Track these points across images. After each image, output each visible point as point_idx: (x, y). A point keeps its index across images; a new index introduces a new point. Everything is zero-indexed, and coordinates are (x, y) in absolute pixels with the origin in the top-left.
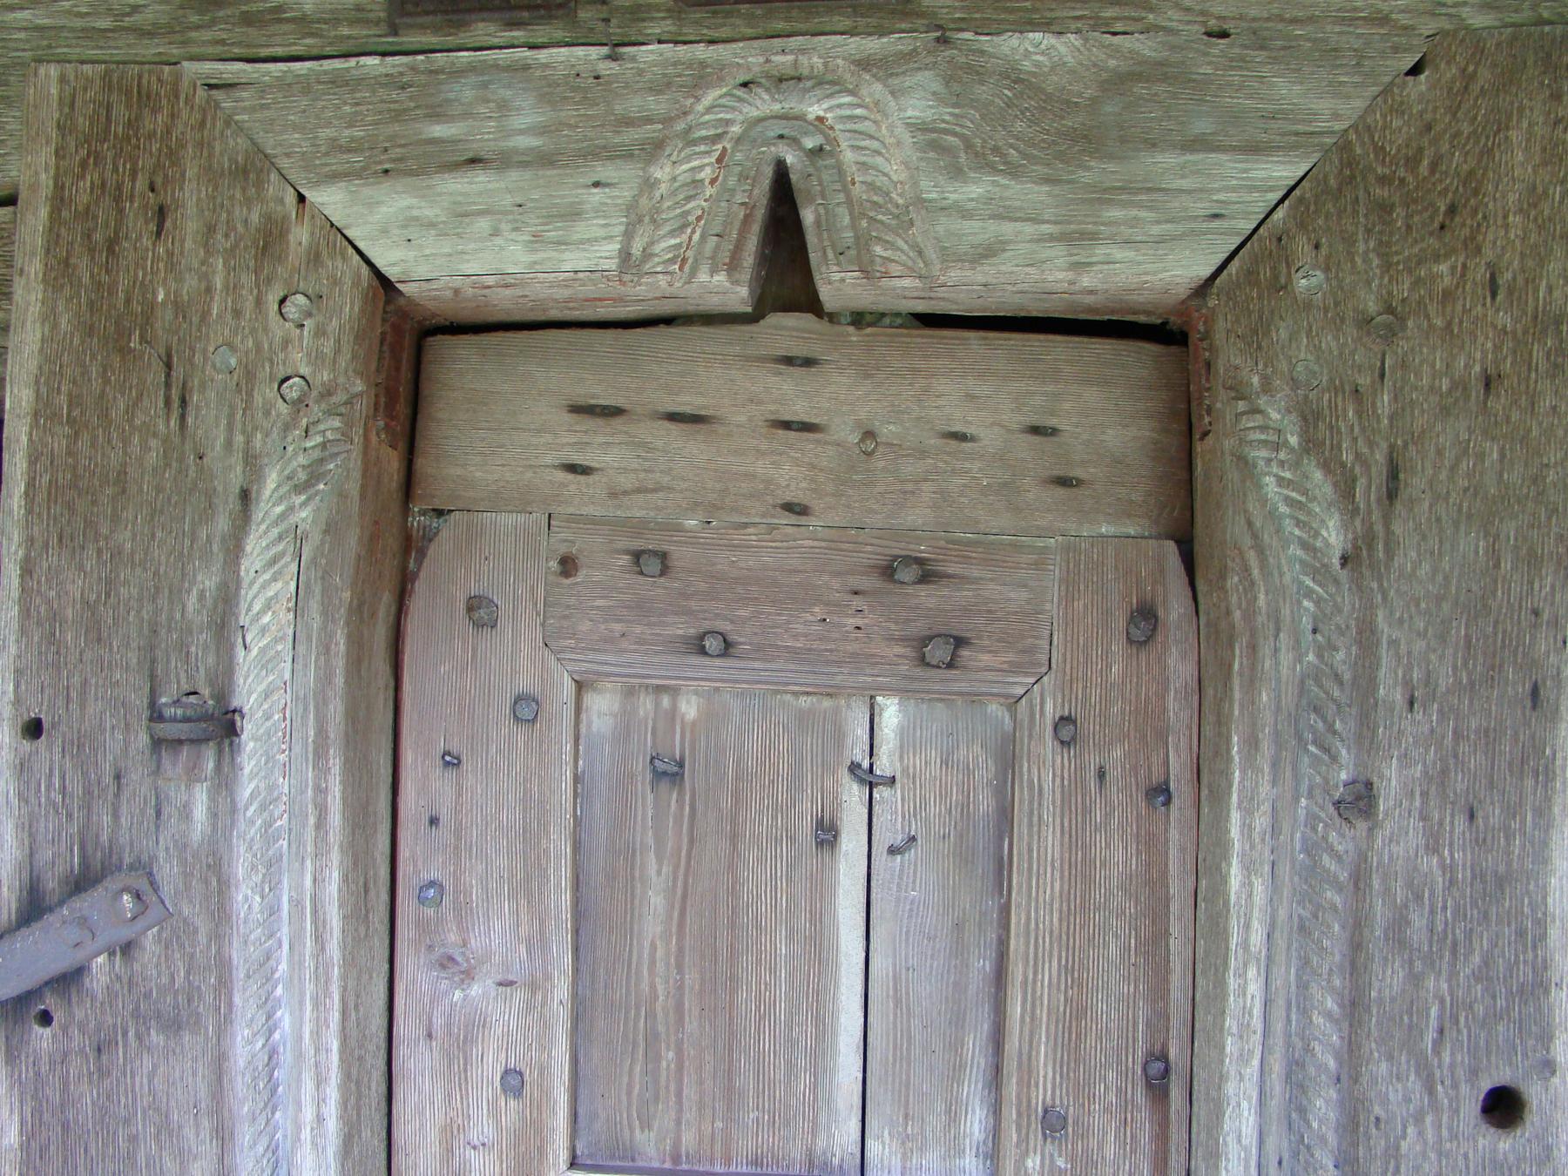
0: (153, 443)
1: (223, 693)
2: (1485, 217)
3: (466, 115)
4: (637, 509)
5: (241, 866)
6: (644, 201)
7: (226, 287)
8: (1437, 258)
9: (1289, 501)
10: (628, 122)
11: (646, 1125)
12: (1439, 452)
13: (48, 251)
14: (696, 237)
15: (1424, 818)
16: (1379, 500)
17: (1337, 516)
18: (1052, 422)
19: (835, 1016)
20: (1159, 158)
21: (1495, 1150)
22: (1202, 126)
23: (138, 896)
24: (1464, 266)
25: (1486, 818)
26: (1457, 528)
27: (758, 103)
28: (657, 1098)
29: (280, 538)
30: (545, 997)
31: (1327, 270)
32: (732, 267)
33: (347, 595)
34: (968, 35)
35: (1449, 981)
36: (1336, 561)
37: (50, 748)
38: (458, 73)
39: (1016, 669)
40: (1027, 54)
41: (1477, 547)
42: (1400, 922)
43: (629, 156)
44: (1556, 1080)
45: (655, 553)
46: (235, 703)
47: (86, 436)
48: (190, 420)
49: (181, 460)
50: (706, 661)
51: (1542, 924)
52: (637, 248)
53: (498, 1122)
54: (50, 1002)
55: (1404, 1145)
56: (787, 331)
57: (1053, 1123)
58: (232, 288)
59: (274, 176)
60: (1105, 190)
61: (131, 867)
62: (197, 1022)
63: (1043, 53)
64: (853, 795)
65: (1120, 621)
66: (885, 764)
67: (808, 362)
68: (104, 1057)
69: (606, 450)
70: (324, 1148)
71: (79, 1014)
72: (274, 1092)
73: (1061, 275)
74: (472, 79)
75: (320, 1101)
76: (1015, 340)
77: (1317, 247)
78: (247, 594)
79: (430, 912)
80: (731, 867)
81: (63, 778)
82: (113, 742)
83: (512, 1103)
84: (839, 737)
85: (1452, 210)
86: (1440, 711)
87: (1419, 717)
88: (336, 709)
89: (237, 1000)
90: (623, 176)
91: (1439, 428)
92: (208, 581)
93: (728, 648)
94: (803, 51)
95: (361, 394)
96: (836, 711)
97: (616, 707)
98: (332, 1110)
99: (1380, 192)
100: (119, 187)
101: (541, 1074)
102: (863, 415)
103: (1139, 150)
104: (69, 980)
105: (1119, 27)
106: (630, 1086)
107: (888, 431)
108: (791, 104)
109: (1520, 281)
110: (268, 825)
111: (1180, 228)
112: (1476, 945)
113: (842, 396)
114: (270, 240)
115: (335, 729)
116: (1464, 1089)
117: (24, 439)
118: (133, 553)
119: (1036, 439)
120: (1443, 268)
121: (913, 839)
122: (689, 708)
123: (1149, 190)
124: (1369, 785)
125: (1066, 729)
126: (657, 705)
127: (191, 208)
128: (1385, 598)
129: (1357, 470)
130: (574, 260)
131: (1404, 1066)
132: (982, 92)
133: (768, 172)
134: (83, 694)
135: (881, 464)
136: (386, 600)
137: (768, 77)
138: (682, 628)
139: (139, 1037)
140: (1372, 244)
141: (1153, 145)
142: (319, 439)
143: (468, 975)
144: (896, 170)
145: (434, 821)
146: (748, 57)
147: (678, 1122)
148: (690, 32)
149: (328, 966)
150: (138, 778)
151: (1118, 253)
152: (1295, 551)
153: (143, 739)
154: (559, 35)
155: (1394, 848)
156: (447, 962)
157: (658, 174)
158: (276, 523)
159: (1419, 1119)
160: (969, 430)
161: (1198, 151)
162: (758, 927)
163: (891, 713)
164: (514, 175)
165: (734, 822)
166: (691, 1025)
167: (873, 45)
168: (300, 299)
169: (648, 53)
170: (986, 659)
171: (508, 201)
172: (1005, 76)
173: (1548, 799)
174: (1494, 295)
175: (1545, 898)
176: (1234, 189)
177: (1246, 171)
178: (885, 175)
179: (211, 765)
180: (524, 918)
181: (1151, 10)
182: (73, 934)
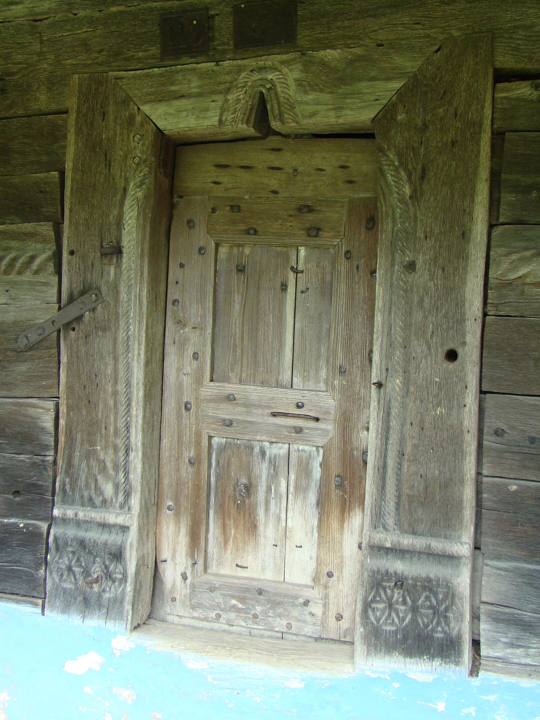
0: (102, 176)
1: (119, 242)
2: (454, 94)
3: (180, 84)
4: (232, 194)
5: (123, 289)
6: (225, 105)
7: (120, 134)
8: (439, 108)
9: (394, 181)
10: (221, 83)
11: (233, 371)
12: (438, 165)
13: (76, 125)
14: (239, 114)
15: (429, 271)
16: (419, 180)
17: (408, 185)
18: (347, 164)
19: (285, 341)
20: (362, 84)
21: (448, 368)
22: (373, 73)
23: (96, 295)
24: (447, 109)
25: (448, 271)
26: (442, 187)
27: (255, 76)
28: (236, 364)
29: (133, 200)
30: (205, 332)
31: (407, 113)
32: (247, 123)
33: (150, 215)
34: (310, 52)
35: (436, 318)
36: (407, 198)
37: (76, 256)
38: (178, 72)
39: (335, 237)
40: (326, 56)
41: (448, 192)
42: (421, 301)
43: (221, 93)
44: (466, 348)
45: (236, 206)
46: (122, 245)
47: (85, 175)
48: (111, 170)
49: (109, 180)
50: (250, 236)
51: (463, 302)
52: (224, 119)
53: (191, 368)
54: (75, 325)
55: (421, 365)
56: (273, 141)
57: (342, 371)
58: (122, 134)
59: (132, 103)
60: (346, 94)
61: (95, 289)
62: (110, 329)
63: (330, 56)
64: (291, 276)
65: (364, 223)
66: (300, 267)
67: (279, 150)
68: (88, 339)
69: (225, 178)
70: (140, 363)
71: (81, 328)
72: (128, 348)
73: (333, 120)
74: (181, 73)
75: (139, 349)
76: (337, 140)
77: (404, 107)
78: (125, 215)
79: (175, 308)
80: (258, 297)
81: (79, 265)
82: (92, 255)
83: (195, 362)
84: (288, 259)
85: (445, 93)
86: (435, 240)
87: (428, 241)
88: (147, 246)
89: (120, 323)
90: (220, 98)
91: (438, 158)
92: (115, 212)
93: (256, 232)
94: (266, 60)
95: (153, 162)
96: (287, 252)
97: (228, 251)
98: (142, 352)
99: (424, 89)
100: (93, 108)
101: (203, 353)
102: (294, 165)
103: (355, 82)
104: (79, 319)
105: (352, 46)
106: (229, 360)
107: (300, 169)
108: (263, 75)
109: (464, 112)
110: (129, 276)
111: (367, 104)
112: (444, 308)
113: (289, 159)
114: (131, 120)
115: (146, 251)
116: (440, 350)
117: (70, 176)
118: (97, 205)
119: (342, 170)
120: (441, 110)
121: (308, 289)
122: (247, 251)
123: (358, 93)
124: (414, 262)
125: (348, 255)
126: (238, 250)
127: (111, 113)
128: (419, 208)
129: (413, 171)
130: (207, 123)
131: (422, 342)
132: (313, 68)
133: (258, 95)
134: (84, 243)
135: (298, 179)
136: (165, 220)
137: (257, 68)
138: (243, 227)
139: (96, 333)
140: (421, 105)
141: (360, 80)
142: (143, 174)
143: (185, 326)
144: (292, 93)
145: (177, 283)
146: (252, 63)
147: (241, 371)
148: (237, 56)
149: (143, 314)
150: (97, 264)
151: (349, 112)
152: (395, 195)
153: (99, 254)
154: (204, 59)
155: (420, 279)
156: (179, 322)
157: (229, 98)
158: (132, 196)
159: (426, 358)
160: (324, 168)
161: (372, 81)
162: (265, 314)
163: (303, 252)
164: (192, 100)
165: (259, 284)
166: (245, 342)
167: (285, 57)
168: (138, 136)
169: (226, 63)
170: (327, 234)
171: (191, 107)
172: (319, 63)
173: (466, 265)
174: (456, 117)
175: (464, 294)
176: (382, 91)
177: (386, 86)
178: (287, 94)
179: (115, 260)
180: (200, 310)
181: (361, 40)
182: (81, 306)
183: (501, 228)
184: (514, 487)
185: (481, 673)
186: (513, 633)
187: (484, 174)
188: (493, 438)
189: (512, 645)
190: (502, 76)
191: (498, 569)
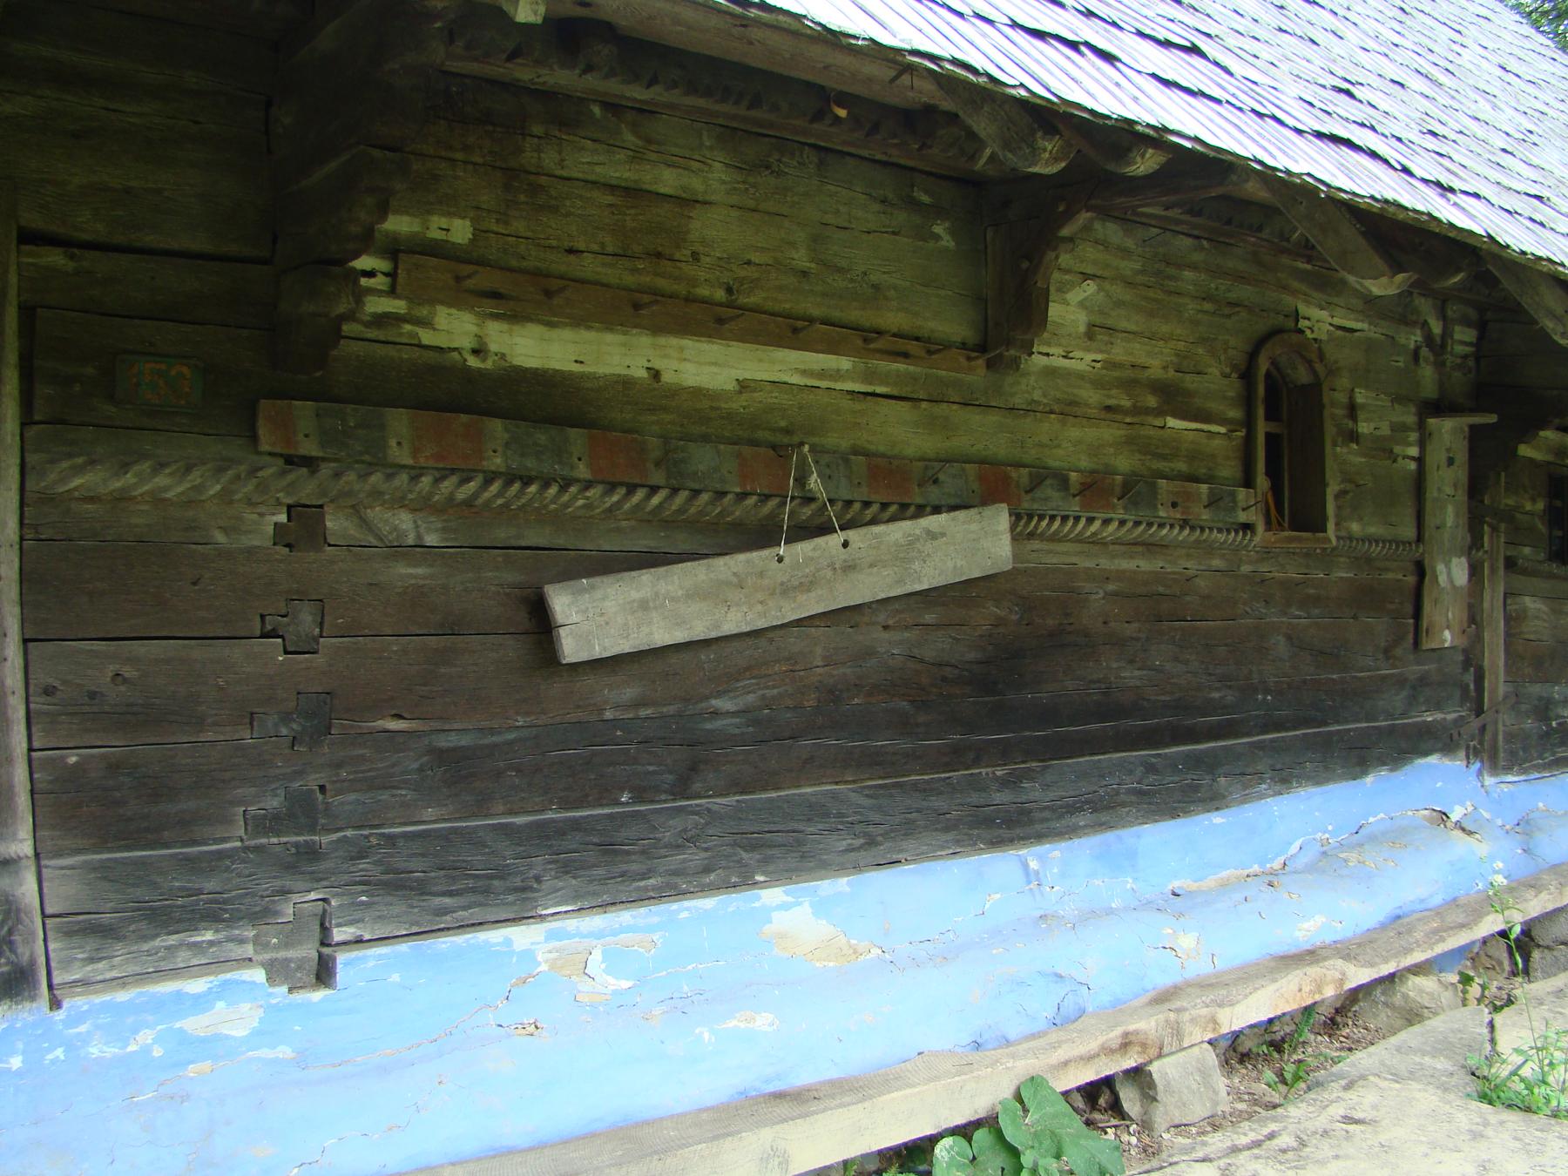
183: (35, 428)
184: (73, 759)
185: (66, 1004)
186: (92, 943)
187: (12, 357)
188: (43, 699)
189: (92, 960)
190: (28, 237)
191: (62, 868)
